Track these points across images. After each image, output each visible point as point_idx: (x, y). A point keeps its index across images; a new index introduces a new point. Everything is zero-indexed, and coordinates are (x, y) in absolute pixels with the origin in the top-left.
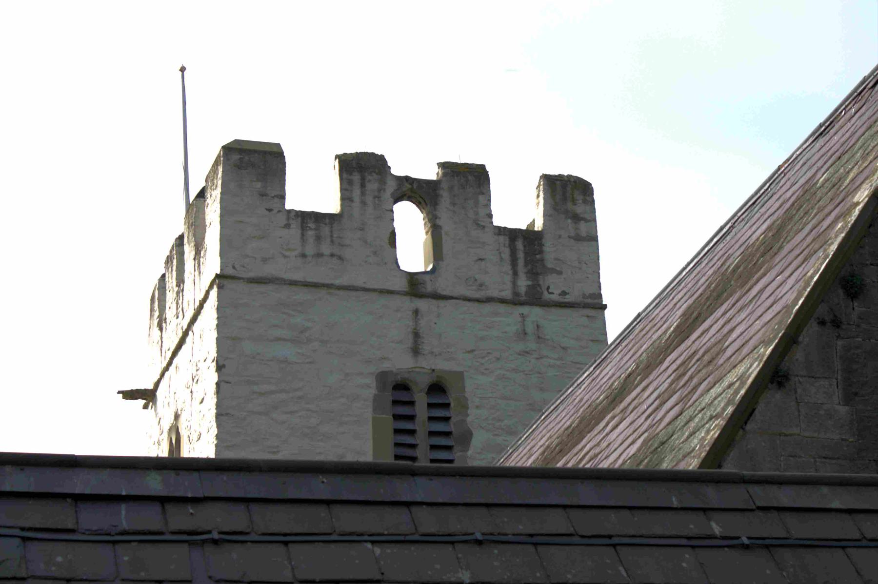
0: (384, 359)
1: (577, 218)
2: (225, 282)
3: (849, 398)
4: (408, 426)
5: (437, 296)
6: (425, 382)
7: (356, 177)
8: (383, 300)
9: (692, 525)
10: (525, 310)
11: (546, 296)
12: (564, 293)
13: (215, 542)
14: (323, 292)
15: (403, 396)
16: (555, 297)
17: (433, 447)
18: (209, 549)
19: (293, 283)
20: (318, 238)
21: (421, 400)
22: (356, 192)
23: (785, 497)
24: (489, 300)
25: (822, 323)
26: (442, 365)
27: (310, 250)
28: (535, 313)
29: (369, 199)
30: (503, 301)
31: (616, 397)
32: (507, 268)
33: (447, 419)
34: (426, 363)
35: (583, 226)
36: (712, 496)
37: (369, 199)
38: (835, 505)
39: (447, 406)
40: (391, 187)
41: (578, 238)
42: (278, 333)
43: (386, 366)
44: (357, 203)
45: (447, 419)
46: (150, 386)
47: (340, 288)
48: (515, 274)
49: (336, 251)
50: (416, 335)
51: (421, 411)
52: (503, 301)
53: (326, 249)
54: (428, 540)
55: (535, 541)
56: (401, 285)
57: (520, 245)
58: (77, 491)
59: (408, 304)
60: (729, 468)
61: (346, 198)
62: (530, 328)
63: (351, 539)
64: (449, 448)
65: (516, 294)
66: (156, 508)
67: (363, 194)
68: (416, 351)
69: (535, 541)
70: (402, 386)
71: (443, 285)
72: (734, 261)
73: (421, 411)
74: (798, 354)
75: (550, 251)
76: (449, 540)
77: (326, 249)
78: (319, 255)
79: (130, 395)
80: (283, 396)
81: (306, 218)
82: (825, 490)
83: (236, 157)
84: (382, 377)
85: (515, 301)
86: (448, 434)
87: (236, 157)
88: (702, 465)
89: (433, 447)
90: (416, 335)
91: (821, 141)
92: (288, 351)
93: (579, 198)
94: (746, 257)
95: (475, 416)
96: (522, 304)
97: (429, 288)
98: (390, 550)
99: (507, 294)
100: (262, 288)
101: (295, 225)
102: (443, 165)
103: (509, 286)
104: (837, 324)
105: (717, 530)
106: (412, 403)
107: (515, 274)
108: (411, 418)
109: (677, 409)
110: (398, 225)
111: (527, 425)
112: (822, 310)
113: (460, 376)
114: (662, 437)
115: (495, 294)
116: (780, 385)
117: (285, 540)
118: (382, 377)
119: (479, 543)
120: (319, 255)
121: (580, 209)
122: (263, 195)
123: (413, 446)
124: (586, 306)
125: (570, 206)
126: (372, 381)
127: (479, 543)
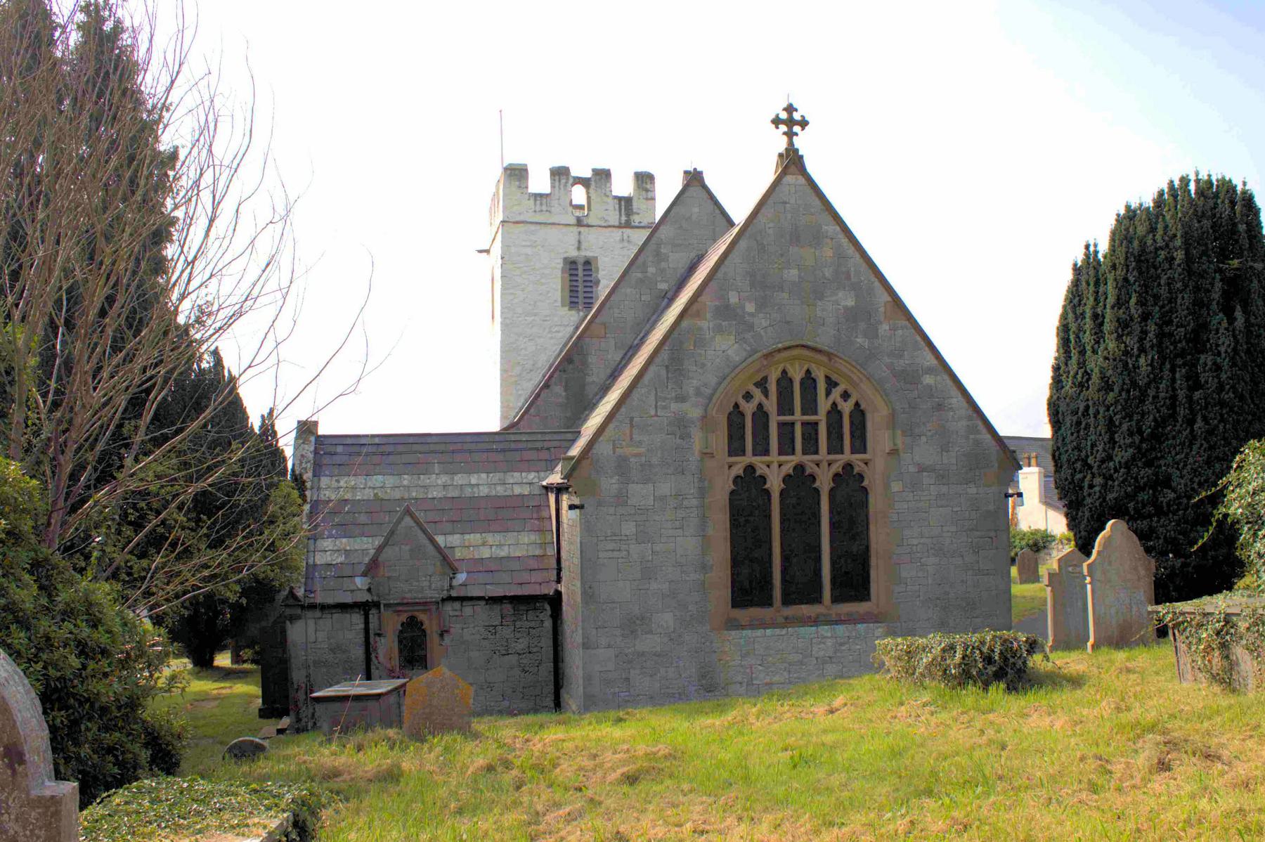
3: (565, 391)
5: (588, 226)
6: (582, 261)
7: (557, 178)
8: (565, 229)
10: (624, 230)
16: (637, 224)
19: (531, 223)
20: (541, 204)
21: (580, 268)
22: (557, 184)
24: (610, 226)
26: (589, 254)
27: (538, 208)
28: (628, 231)
30: (614, 227)
32: (617, 213)
34: (583, 253)
39: (591, 270)
40: (571, 181)
41: (647, 199)
43: (566, 255)
48: (620, 215)
50: (579, 242)
51: (580, 272)
52: (614, 227)
53: (544, 208)
57: (623, 203)
59: (575, 229)
61: (553, 187)
62: (625, 237)
68: (579, 248)
71: (591, 221)
73: (580, 272)
74: (553, 379)
75: (635, 205)
77: (544, 208)
79: (480, 251)
84: (565, 259)
85: (620, 227)
90: (579, 242)
92: (529, 251)
102: (594, 170)
106: (577, 269)
112: (561, 368)
115: (611, 223)
118: (565, 259)
121: (648, 186)
126: (561, 261)
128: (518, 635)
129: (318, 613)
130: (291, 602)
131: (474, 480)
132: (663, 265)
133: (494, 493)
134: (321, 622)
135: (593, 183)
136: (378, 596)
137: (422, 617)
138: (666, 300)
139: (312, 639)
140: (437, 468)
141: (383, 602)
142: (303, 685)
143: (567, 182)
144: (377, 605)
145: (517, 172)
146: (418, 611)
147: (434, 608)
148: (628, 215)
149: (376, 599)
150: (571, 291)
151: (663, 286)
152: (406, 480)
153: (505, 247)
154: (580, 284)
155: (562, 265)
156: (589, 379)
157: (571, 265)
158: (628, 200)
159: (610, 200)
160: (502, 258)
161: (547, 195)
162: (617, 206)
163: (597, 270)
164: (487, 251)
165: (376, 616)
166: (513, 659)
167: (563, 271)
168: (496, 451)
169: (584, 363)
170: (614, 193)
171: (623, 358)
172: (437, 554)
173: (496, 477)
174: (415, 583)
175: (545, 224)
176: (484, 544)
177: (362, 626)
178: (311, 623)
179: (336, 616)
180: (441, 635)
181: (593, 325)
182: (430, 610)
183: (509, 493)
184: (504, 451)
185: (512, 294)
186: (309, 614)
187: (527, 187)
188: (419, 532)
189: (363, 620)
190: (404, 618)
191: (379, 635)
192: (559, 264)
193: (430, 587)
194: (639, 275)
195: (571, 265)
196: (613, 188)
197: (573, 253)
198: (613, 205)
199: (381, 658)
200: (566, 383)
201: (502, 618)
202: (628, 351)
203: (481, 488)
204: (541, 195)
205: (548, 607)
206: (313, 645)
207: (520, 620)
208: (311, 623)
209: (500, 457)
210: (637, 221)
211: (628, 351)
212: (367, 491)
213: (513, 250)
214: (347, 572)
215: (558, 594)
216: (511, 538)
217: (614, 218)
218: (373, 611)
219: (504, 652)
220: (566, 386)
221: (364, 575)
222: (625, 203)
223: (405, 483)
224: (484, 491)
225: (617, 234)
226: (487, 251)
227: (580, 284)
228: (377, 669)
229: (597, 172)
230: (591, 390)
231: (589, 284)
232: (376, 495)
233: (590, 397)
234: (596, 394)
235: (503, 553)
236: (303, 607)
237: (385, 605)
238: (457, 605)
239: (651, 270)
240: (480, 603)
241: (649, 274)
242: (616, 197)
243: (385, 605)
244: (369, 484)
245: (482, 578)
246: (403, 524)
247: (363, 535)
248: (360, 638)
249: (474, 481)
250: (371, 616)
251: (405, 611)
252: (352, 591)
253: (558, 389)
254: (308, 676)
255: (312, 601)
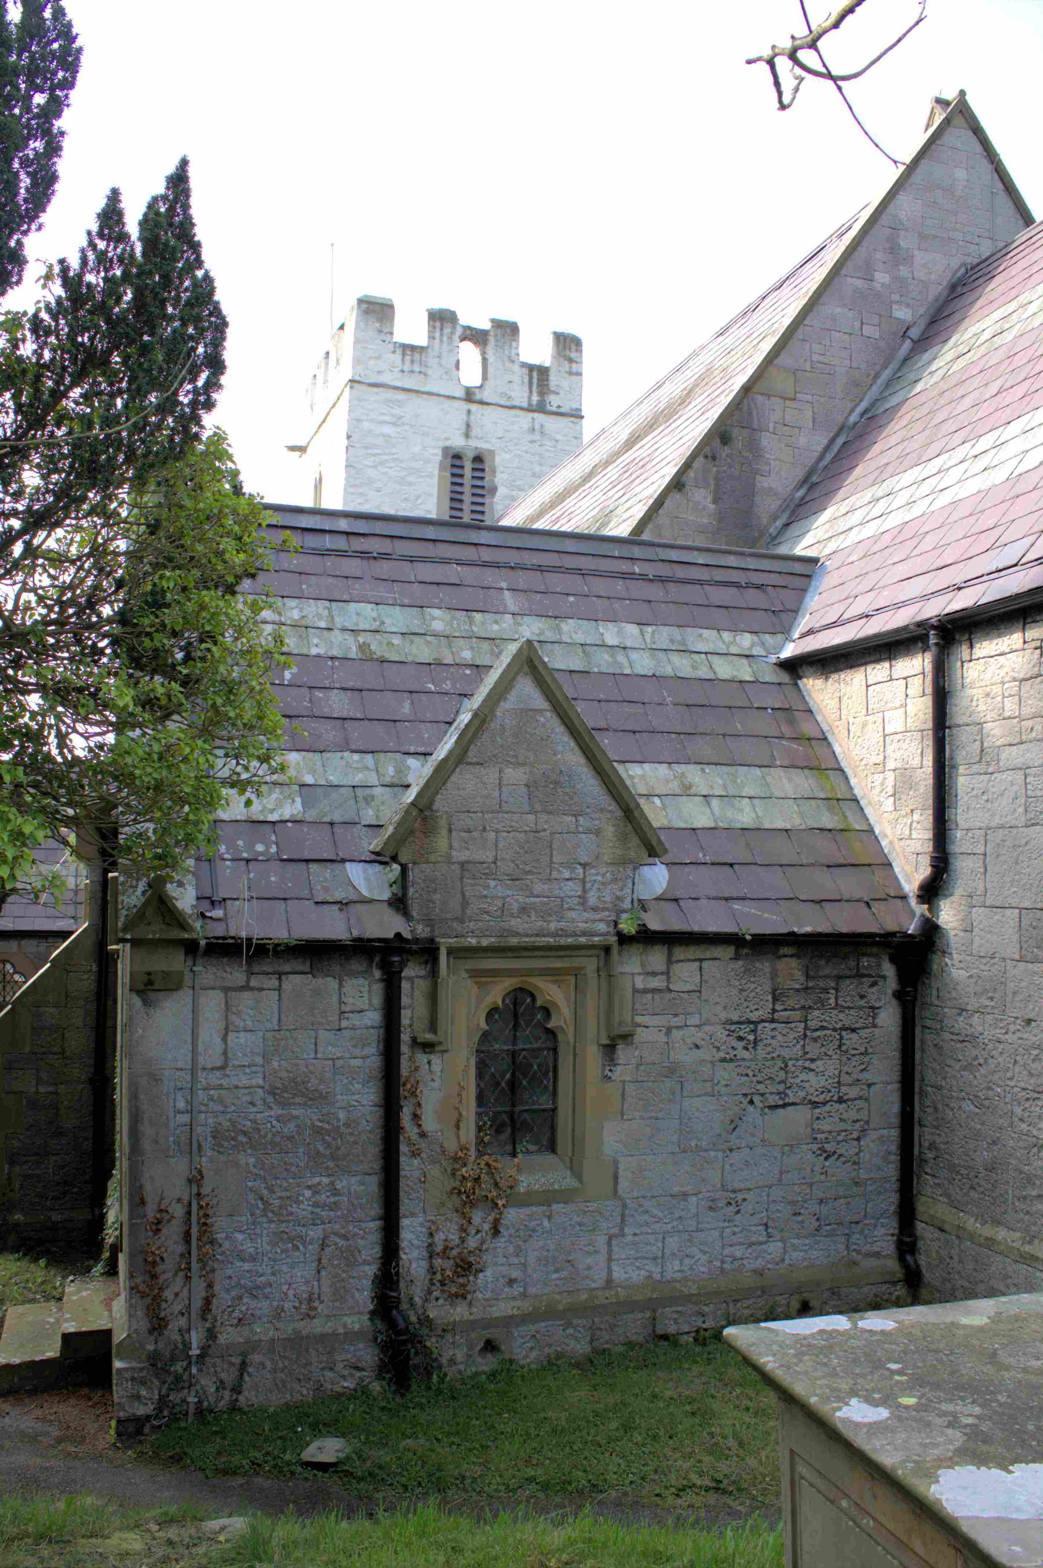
0: (447, 439)
1: (571, 361)
2: (356, 385)
3: (715, 501)
4: (459, 480)
5: (482, 403)
6: (471, 455)
7: (438, 324)
8: (448, 403)
9: (624, 566)
10: (536, 415)
11: (549, 408)
12: (559, 407)
13: (375, 558)
14: (414, 395)
15: (458, 463)
16: (554, 409)
17: (473, 495)
18: (372, 561)
20: (412, 362)
21: (468, 466)
22: (437, 334)
23: (674, 555)
24: (513, 407)
25: (706, 457)
26: (484, 446)
27: (406, 368)
28: (540, 417)
29: (445, 339)
30: (521, 408)
31: (587, 478)
32: (526, 388)
33: (482, 478)
34: (474, 443)
35: (574, 365)
36: (637, 552)
37: (445, 339)
38: (701, 562)
39: (483, 470)
40: (459, 332)
41: (570, 373)
42: (387, 418)
43: (448, 443)
44: (437, 341)
45: (482, 478)
46: (304, 444)
47: (423, 393)
48: (531, 392)
49: (423, 370)
50: (468, 426)
51: (468, 472)
52: (521, 408)
53: (417, 368)
54: (485, 565)
55: (540, 569)
56: (460, 393)
57: (535, 374)
58: (304, 526)
59: (465, 406)
60: (646, 537)
61: (431, 337)
62: (537, 427)
63: (445, 561)
64: (483, 496)
65: (530, 404)
66: (344, 537)
67: (442, 335)
68: (467, 435)
69: (540, 569)
70: (457, 456)
71: (486, 395)
72: (662, 406)
73: (468, 472)
74: (691, 474)
75: (553, 380)
76: (496, 565)
77: (417, 368)
78: (412, 372)
79: (292, 449)
80: (386, 457)
81: (405, 347)
82: (696, 553)
83: (364, 306)
84: (446, 450)
85: (530, 409)
86: (483, 487)
87: (364, 306)
88: (632, 533)
89: (473, 495)
90: (468, 426)
91: (721, 338)
92: (387, 429)
93: (574, 348)
94: (669, 406)
95: (500, 479)
96: (533, 411)
97: (478, 397)
98: (465, 568)
99: (525, 405)
100: (375, 390)
101: (399, 351)
102: (493, 321)
103: (526, 400)
104: (714, 458)
105: (637, 570)
106: (462, 467)
107: (531, 392)
108: (461, 476)
109: (621, 493)
110: (462, 357)
111: (532, 486)
112: (707, 450)
113: (492, 453)
114: (611, 508)
115: (517, 404)
116: (680, 490)
117: (412, 560)
118: (446, 450)
119: (512, 568)
120: (412, 372)
121: (573, 355)
122: (380, 331)
123: (462, 493)
124: (572, 416)
125: (567, 353)
126: (439, 452)
127: (512, 568)
128: (814, 1050)
129: (236, 975)
130: (155, 931)
131: (610, 634)
132: (904, 271)
133: (668, 671)
134: (247, 998)
135: (491, 339)
136: (429, 922)
137: (551, 992)
138: (907, 345)
139: (211, 1055)
140: (510, 600)
141: (444, 943)
142: (178, 1211)
143: (452, 333)
144: (428, 952)
145: (377, 308)
146: (544, 973)
147: (590, 965)
148: (541, 394)
149: (422, 931)
150: (452, 499)
151: (903, 314)
152: (438, 620)
153: (355, 422)
154: (467, 490)
155: (439, 458)
156: (763, 482)
157: (454, 459)
158: (542, 372)
159: (516, 368)
160: (349, 437)
161: (422, 348)
162: (526, 380)
163: (494, 472)
164: (302, 449)
165: (422, 986)
166: (800, 1115)
167: (442, 467)
168: (643, 577)
169: (754, 446)
170: (524, 358)
171: (827, 448)
172: (613, 806)
173: (664, 636)
174: (539, 888)
175: (417, 392)
176: (687, 791)
177: (374, 1017)
178: (212, 1003)
179: (292, 983)
180: (610, 1049)
181: (771, 368)
182: (577, 973)
183: (704, 673)
184: (662, 580)
185: (361, 494)
186: (208, 973)
187: (392, 333)
188: (559, 731)
189: (378, 1000)
190: (497, 994)
191: (428, 1047)
192: (436, 456)
193: (583, 899)
194: (859, 283)
195: (454, 459)
196: (521, 350)
197: (458, 442)
198: (519, 375)
199: (429, 1123)
200: (717, 485)
201: (775, 999)
202: (837, 435)
203: (634, 656)
204: (413, 348)
205: (889, 970)
206: (215, 1078)
207: (822, 1004)
208: (212, 1003)
209: (655, 592)
210: (555, 404)
211: (837, 435)
212: (337, 637)
213: (366, 425)
214: (316, 844)
215: (931, 930)
216: (749, 780)
217: (520, 395)
218: (412, 972)
219: (774, 1100)
220: (716, 492)
221: (379, 858)
222: (539, 375)
223: (438, 626)
224: (643, 664)
225: (525, 420)
226: (302, 449)
227: (467, 490)
228: (415, 1154)
229: (499, 325)
230: (766, 507)
231: (479, 491)
232: (363, 647)
233: (765, 521)
234: (775, 518)
235: (745, 816)
236: (191, 948)
237: (450, 952)
238: (657, 957)
239: (882, 278)
240: (718, 951)
241: (877, 286)
242: (524, 365)
243: (450, 952)
244: (339, 621)
245: (705, 880)
246: (510, 703)
247: (345, 746)
248: (370, 1057)
249: (611, 639)
250: (405, 985)
251: (510, 973)
252: (343, 905)
253: (702, 497)
254: (196, 1179)
255: (219, 930)
